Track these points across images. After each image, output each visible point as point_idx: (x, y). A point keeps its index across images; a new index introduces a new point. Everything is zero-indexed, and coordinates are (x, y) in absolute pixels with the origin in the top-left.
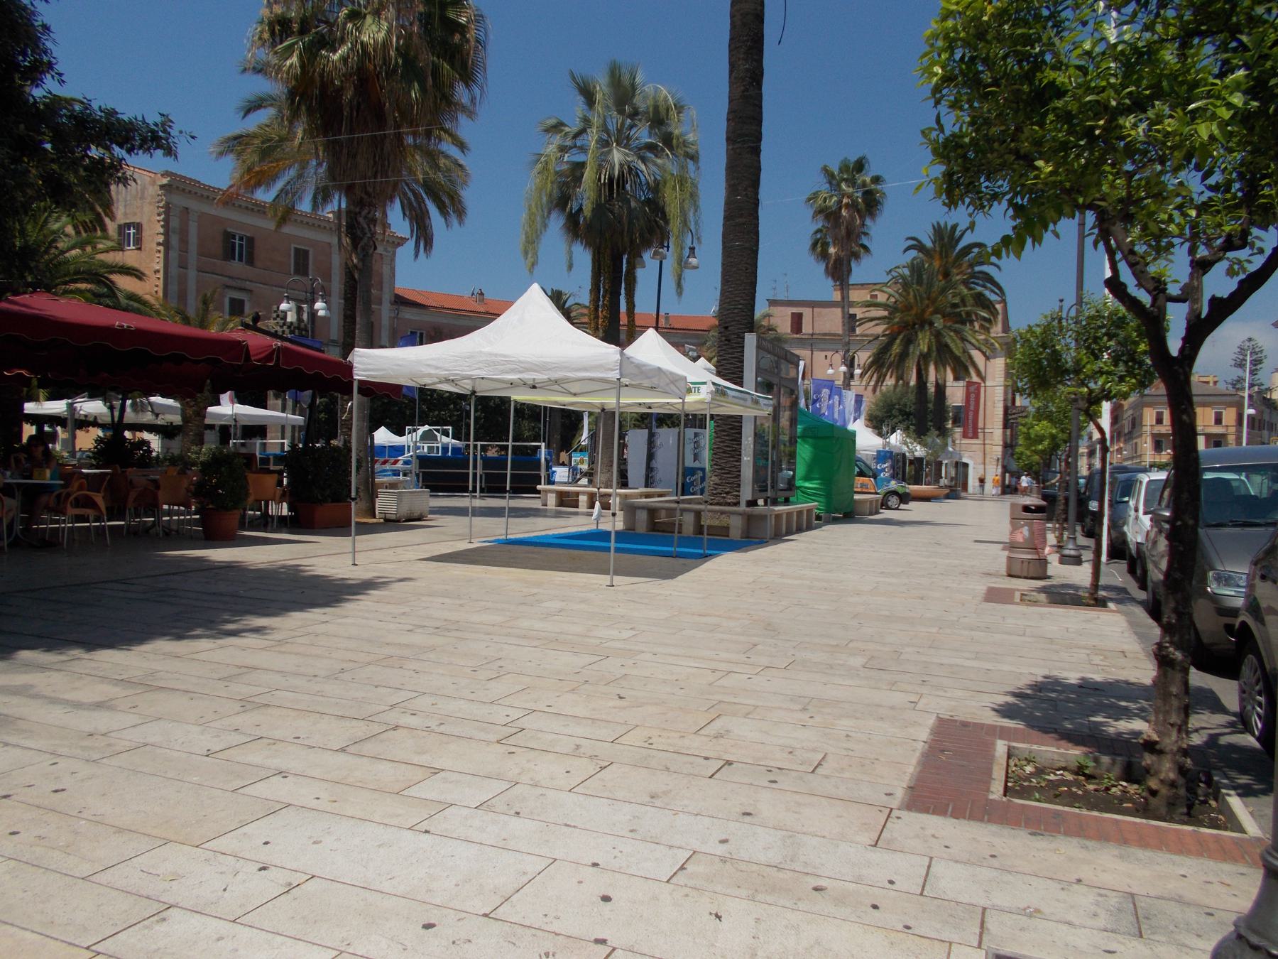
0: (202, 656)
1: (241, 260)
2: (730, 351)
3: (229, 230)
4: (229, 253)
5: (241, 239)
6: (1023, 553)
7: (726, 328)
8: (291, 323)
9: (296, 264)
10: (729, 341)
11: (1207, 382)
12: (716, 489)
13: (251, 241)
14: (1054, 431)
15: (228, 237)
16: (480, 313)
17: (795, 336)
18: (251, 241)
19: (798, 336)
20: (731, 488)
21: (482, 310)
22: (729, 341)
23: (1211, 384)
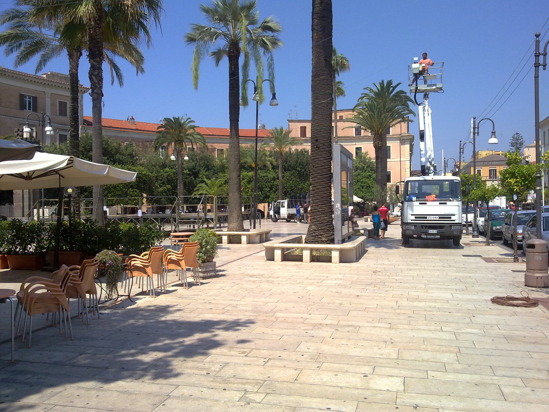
0: (247, 317)
1: (29, 109)
2: (320, 153)
3: (22, 93)
4: (22, 107)
5: (30, 97)
6: (537, 273)
7: (317, 140)
8: (26, 138)
9: (60, 110)
10: (318, 148)
11: (499, 154)
12: (315, 233)
13: (35, 99)
14: (216, 187)
15: (22, 97)
16: (132, 129)
17: (303, 138)
18: (35, 99)
19: (304, 138)
20: (323, 232)
21: (134, 128)
22: (318, 148)
23: (501, 155)
